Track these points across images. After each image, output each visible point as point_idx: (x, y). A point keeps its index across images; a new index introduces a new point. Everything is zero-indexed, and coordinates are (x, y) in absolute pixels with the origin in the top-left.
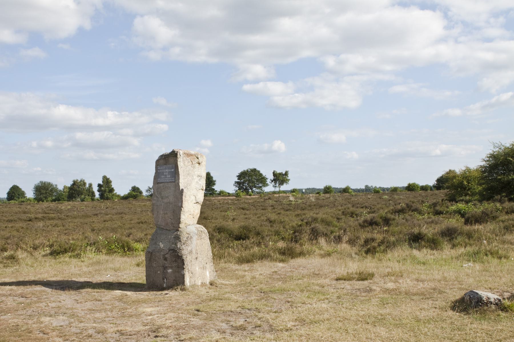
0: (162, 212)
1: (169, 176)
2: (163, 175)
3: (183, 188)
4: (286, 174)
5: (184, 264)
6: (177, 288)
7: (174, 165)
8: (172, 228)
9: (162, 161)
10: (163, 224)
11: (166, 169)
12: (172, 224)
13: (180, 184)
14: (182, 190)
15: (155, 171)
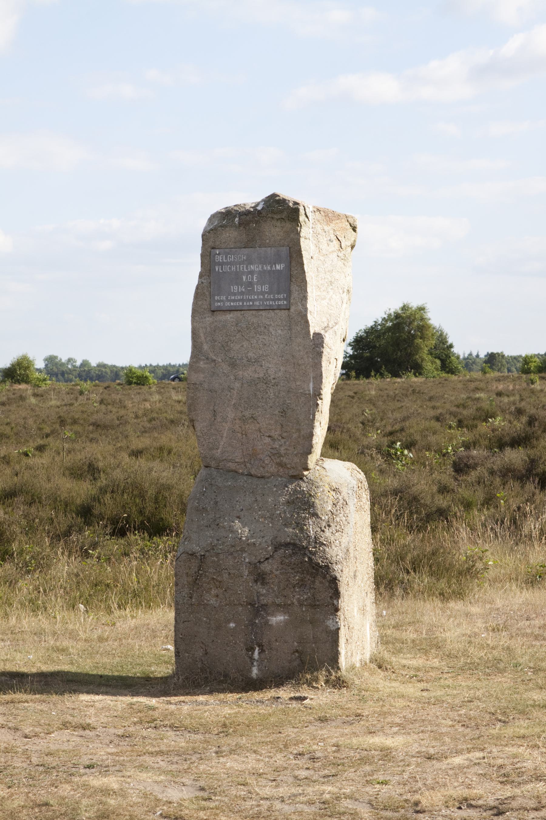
0: (231, 415)
1: (266, 288)
2: (239, 283)
3: (318, 330)
4: (471, 352)
5: (337, 594)
6: (317, 680)
7: (284, 251)
8: (273, 469)
9: (231, 235)
10: (238, 456)
11: (249, 261)
12: (275, 454)
13: (309, 317)
14: (319, 337)
15: (198, 269)
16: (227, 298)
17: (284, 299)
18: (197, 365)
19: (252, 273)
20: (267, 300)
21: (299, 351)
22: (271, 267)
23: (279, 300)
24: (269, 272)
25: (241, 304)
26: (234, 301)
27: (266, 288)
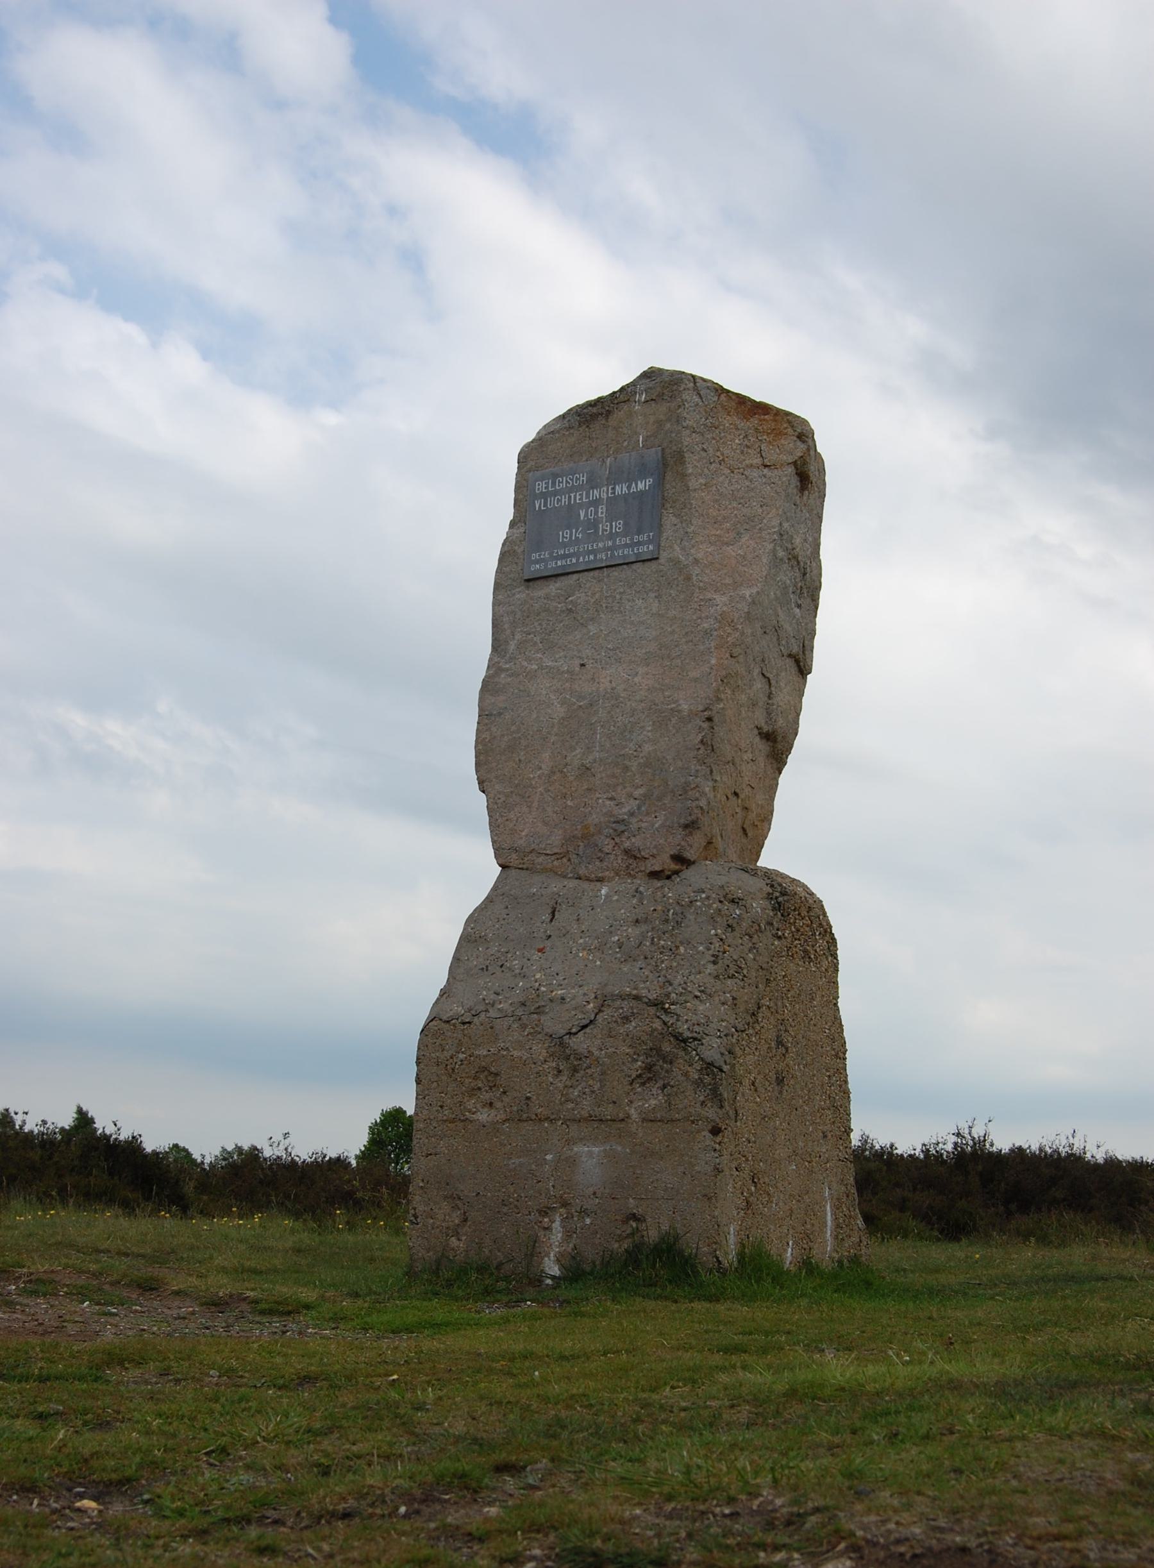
1: (618, 526)
4: (80, 1111)
15: (509, 514)
16: (551, 554)
17: (650, 542)
18: (496, 679)
19: (596, 503)
20: (620, 547)
21: (673, 632)
22: (629, 488)
23: (639, 543)
24: (625, 497)
25: (574, 561)
26: (564, 557)
27: (618, 526)
